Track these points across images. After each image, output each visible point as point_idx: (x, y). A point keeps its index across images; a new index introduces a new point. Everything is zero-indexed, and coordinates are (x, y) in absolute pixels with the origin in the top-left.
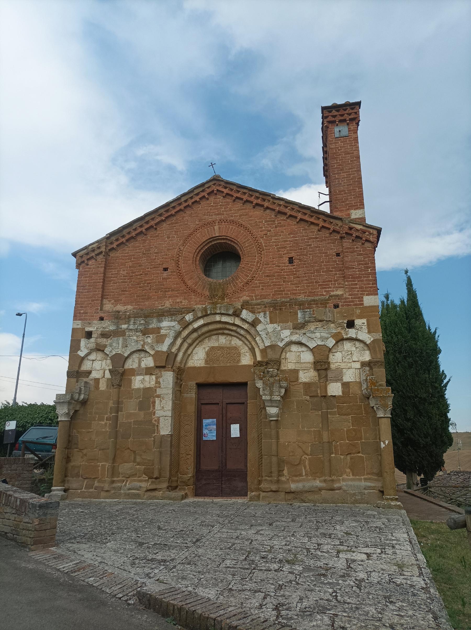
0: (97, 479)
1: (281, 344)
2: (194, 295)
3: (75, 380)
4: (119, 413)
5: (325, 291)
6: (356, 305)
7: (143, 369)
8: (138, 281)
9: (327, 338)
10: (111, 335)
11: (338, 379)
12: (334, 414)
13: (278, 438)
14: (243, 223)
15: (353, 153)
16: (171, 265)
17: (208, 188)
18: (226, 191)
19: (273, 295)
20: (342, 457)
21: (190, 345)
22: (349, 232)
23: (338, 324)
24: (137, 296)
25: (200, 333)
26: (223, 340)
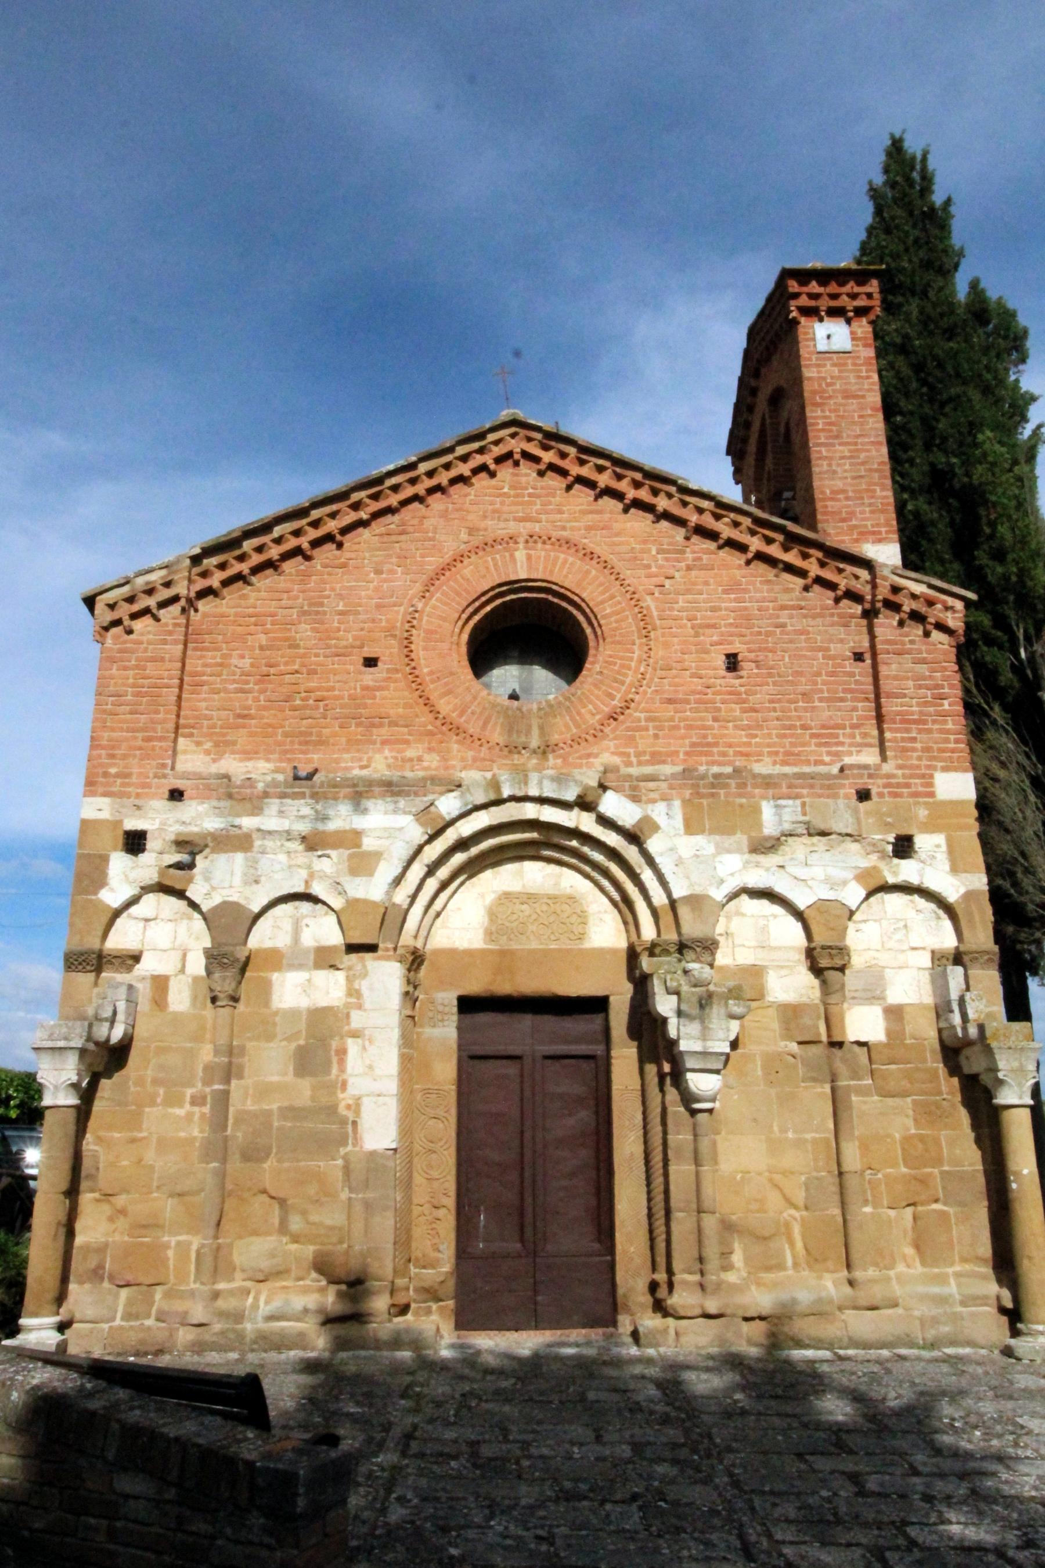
0: (159, 1288)
2: (458, 742)
3: (91, 976)
4: (234, 1082)
5: (829, 753)
6: (916, 795)
7: (307, 951)
8: (285, 690)
9: (845, 883)
10: (206, 846)
11: (873, 995)
12: (862, 1092)
14: (598, 550)
15: (863, 397)
17: (497, 443)
18: (548, 457)
19: (687, 753)
20: (892, 1213)
21: (444, 886)
22: (892, 598)
23: (869, 844)
24: (286, 735)
25: (474, 851)
26: (533, 875)
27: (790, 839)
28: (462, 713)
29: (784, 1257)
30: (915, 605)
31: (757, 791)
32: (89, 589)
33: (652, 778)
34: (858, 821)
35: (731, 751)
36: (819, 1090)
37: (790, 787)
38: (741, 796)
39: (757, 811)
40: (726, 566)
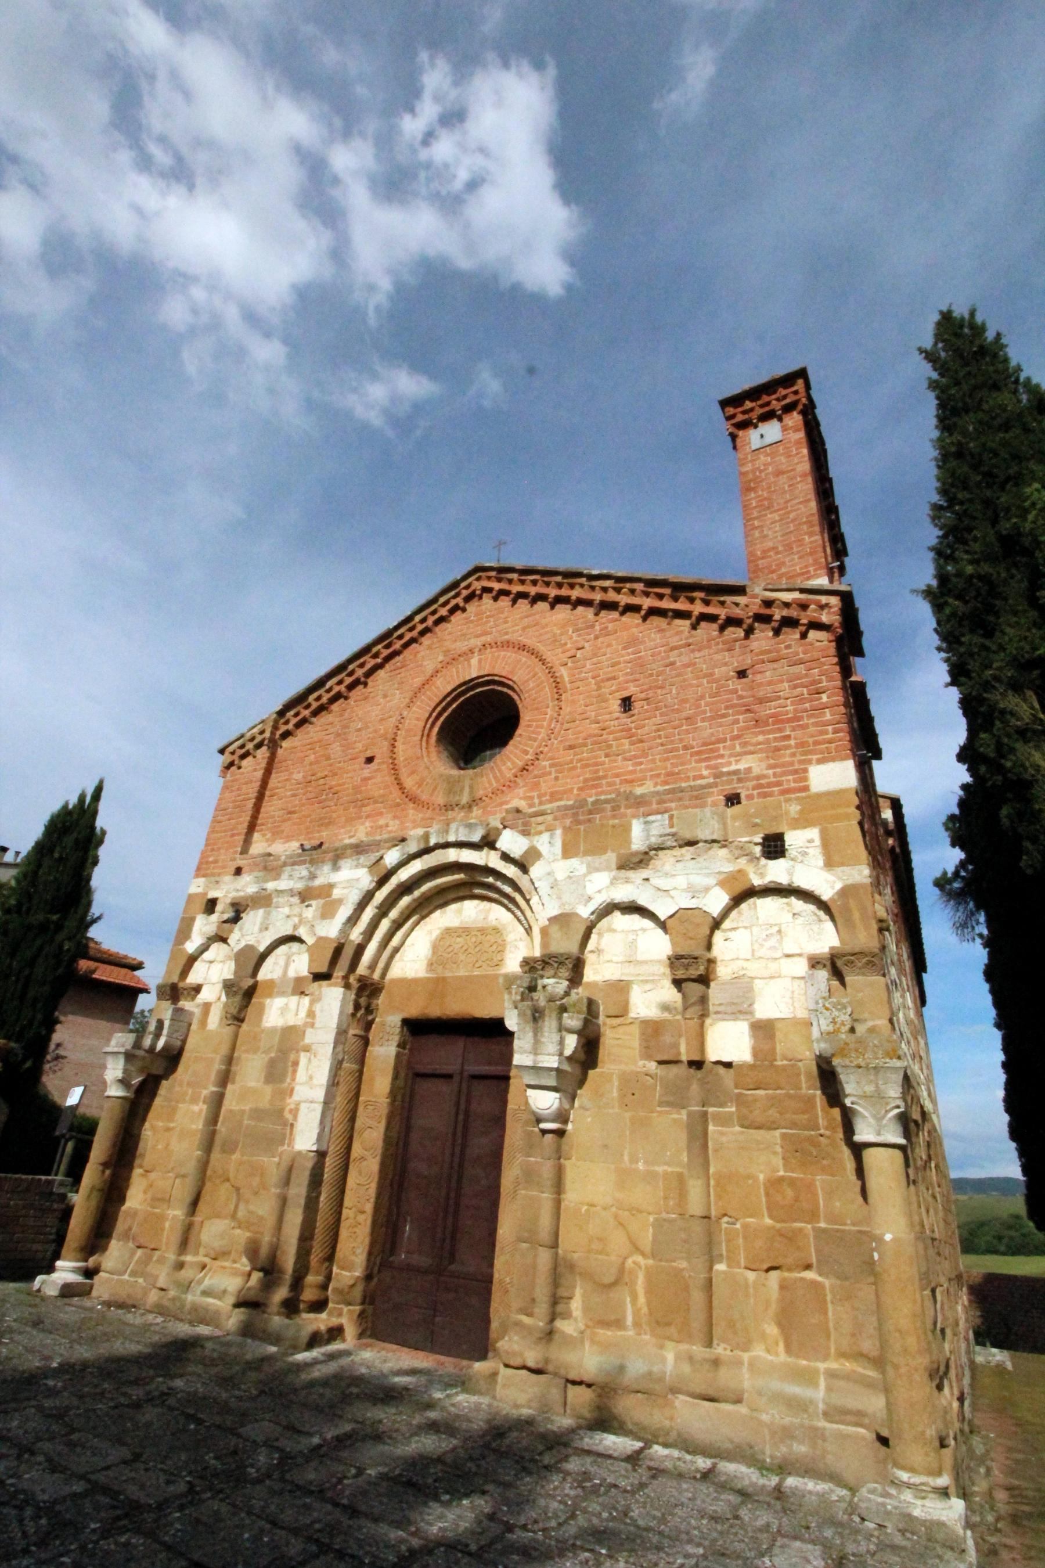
1: (585, 912)
5: (707, 767)
6: (783, 792)
9: (707, 889)
11: (740, 1010)
12: (724, 1121)
13: (559, 1186)
16: (380, 751)
20: (751, 1276)
21: (397, 925)
23: (737, 847)
27: (660, 853)
28: (420, 786)
29: (624, 1312)
30: (785, 612)
31: (629, 811)
32: (220, 745)
33: (542, 814)
34: (725, 824)
35: (617, 780)
36: (675, 1116)
37: (659, 803)
38: (614, 817)
39: (627, 829)
40: (626, 628)
